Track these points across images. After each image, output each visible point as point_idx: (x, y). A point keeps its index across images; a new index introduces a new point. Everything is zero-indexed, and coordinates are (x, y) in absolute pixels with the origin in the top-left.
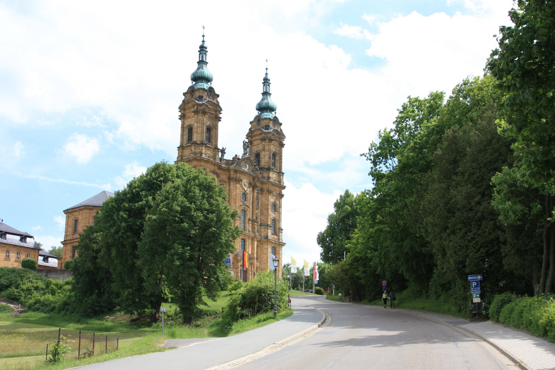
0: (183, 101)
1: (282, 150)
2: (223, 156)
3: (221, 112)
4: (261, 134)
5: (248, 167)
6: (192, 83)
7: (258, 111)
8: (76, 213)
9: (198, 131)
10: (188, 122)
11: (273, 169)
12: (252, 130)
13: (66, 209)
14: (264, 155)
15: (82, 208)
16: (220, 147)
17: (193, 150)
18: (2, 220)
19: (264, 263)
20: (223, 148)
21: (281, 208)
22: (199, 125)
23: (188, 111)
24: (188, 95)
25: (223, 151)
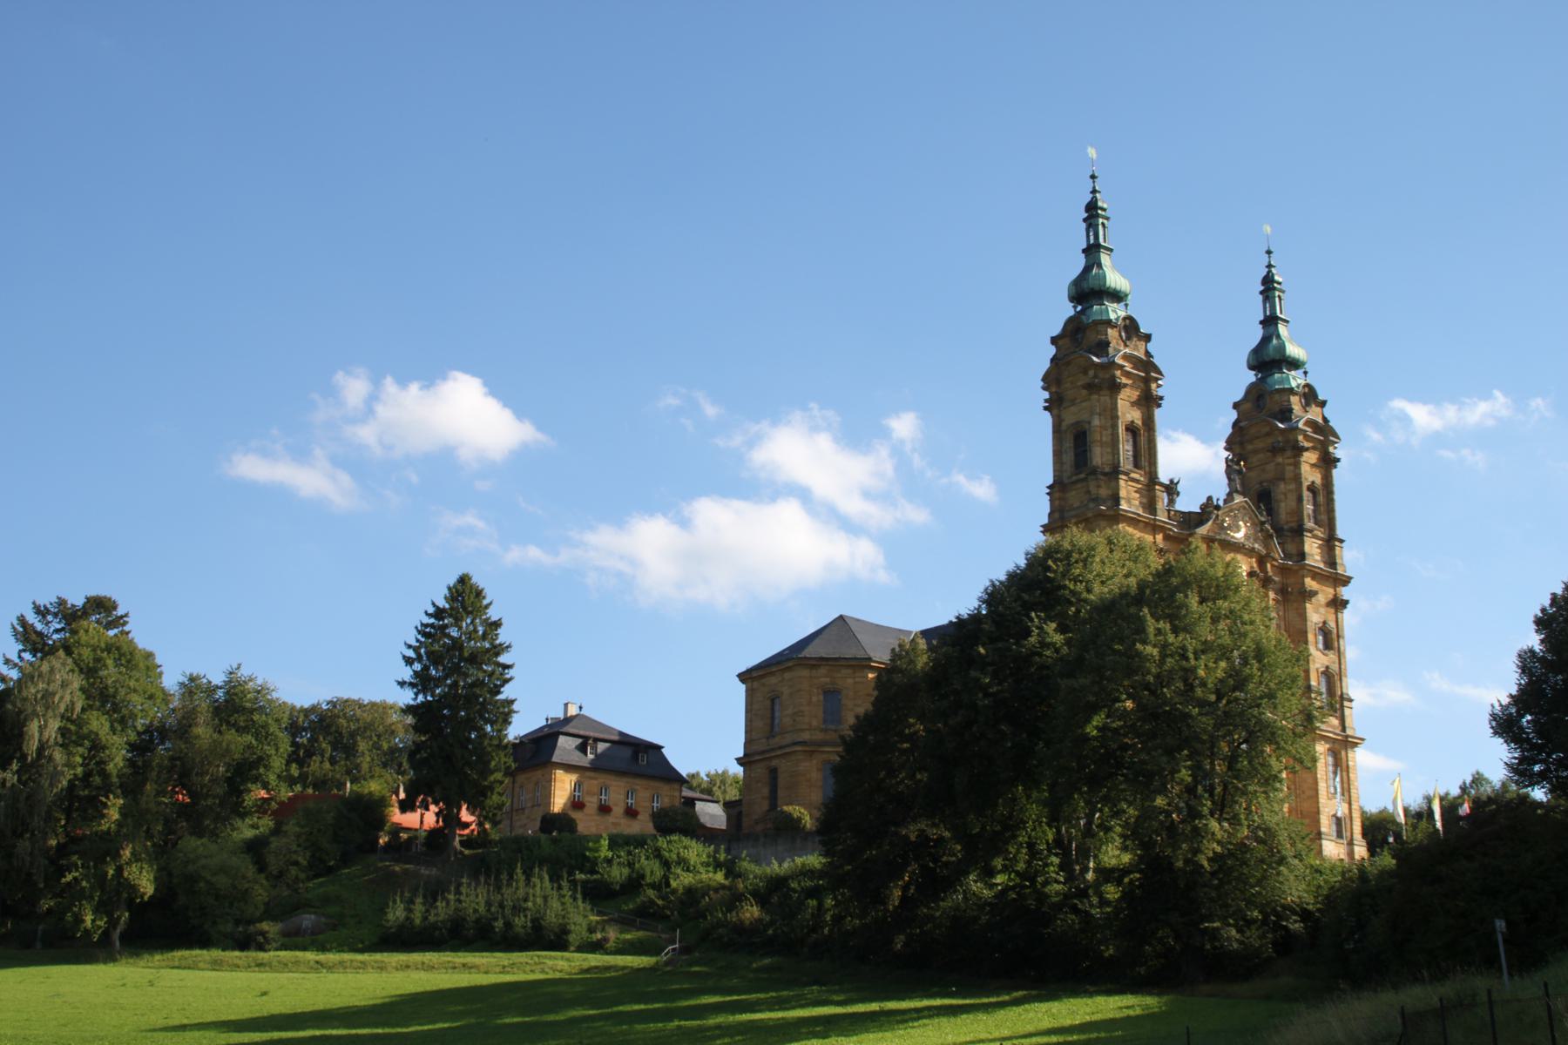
0: (1052, 360)
1: (1331, 476)
2: (1171, 502)
4: (1268, 434)
6: (1075, 307)
7: (1254, 372)
8: (773, 680)
9: (1104, 439)
10: (1070, 417)
11: (1310, 531)
12: (1242, 424)
13: (744, 669)
14: (1285, 494)
15: (790, 664)
16: (1164, 476)
18: (581, 708)
19: (1309, 798)
20: (1172, 481)
21: (1343, 638)
24: (1065, 342)
25: (1172, 489)
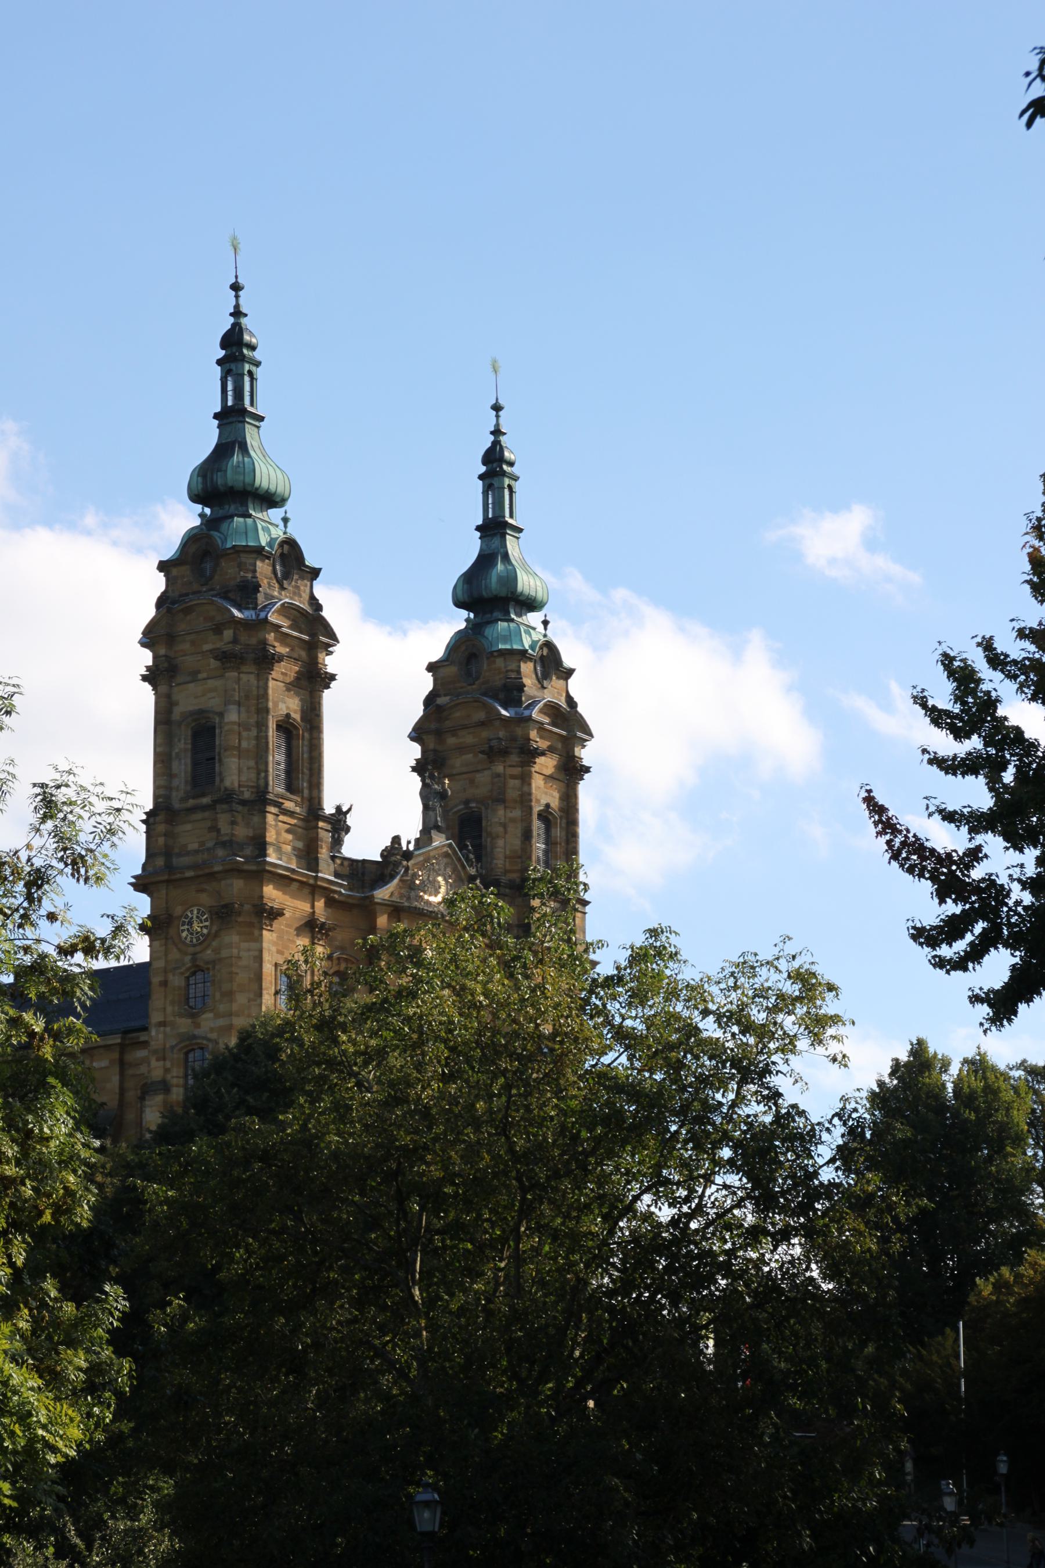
1: (576, 796)
3: (331, 649)
4: (482, 724)
5: (443, 890)
10: (188, 699)
17: (225, 828)
22: (244, 715)
23: (186, 646)
24: (183, 572)
25: (339, 823)
